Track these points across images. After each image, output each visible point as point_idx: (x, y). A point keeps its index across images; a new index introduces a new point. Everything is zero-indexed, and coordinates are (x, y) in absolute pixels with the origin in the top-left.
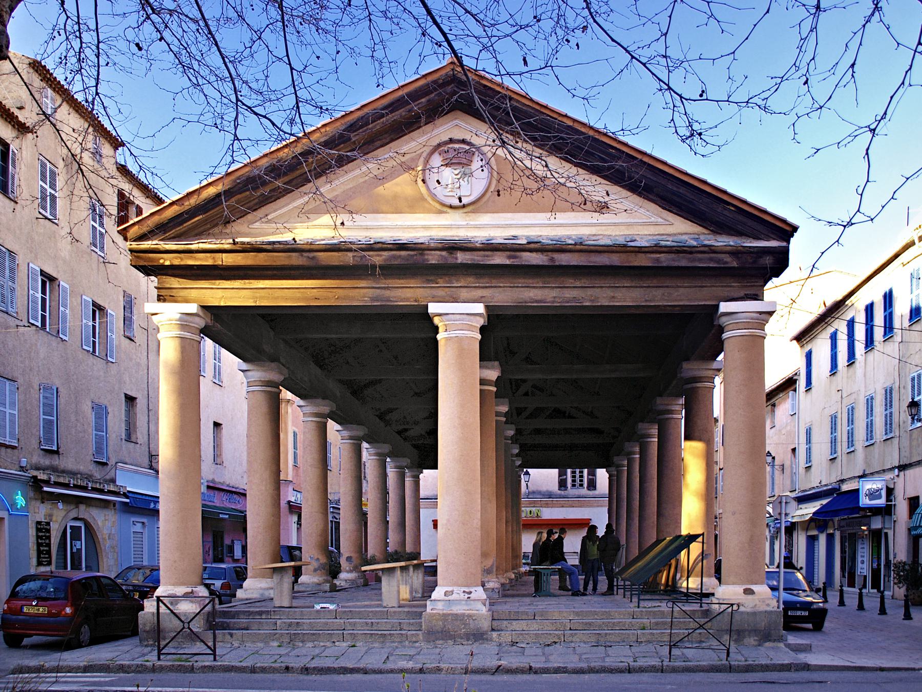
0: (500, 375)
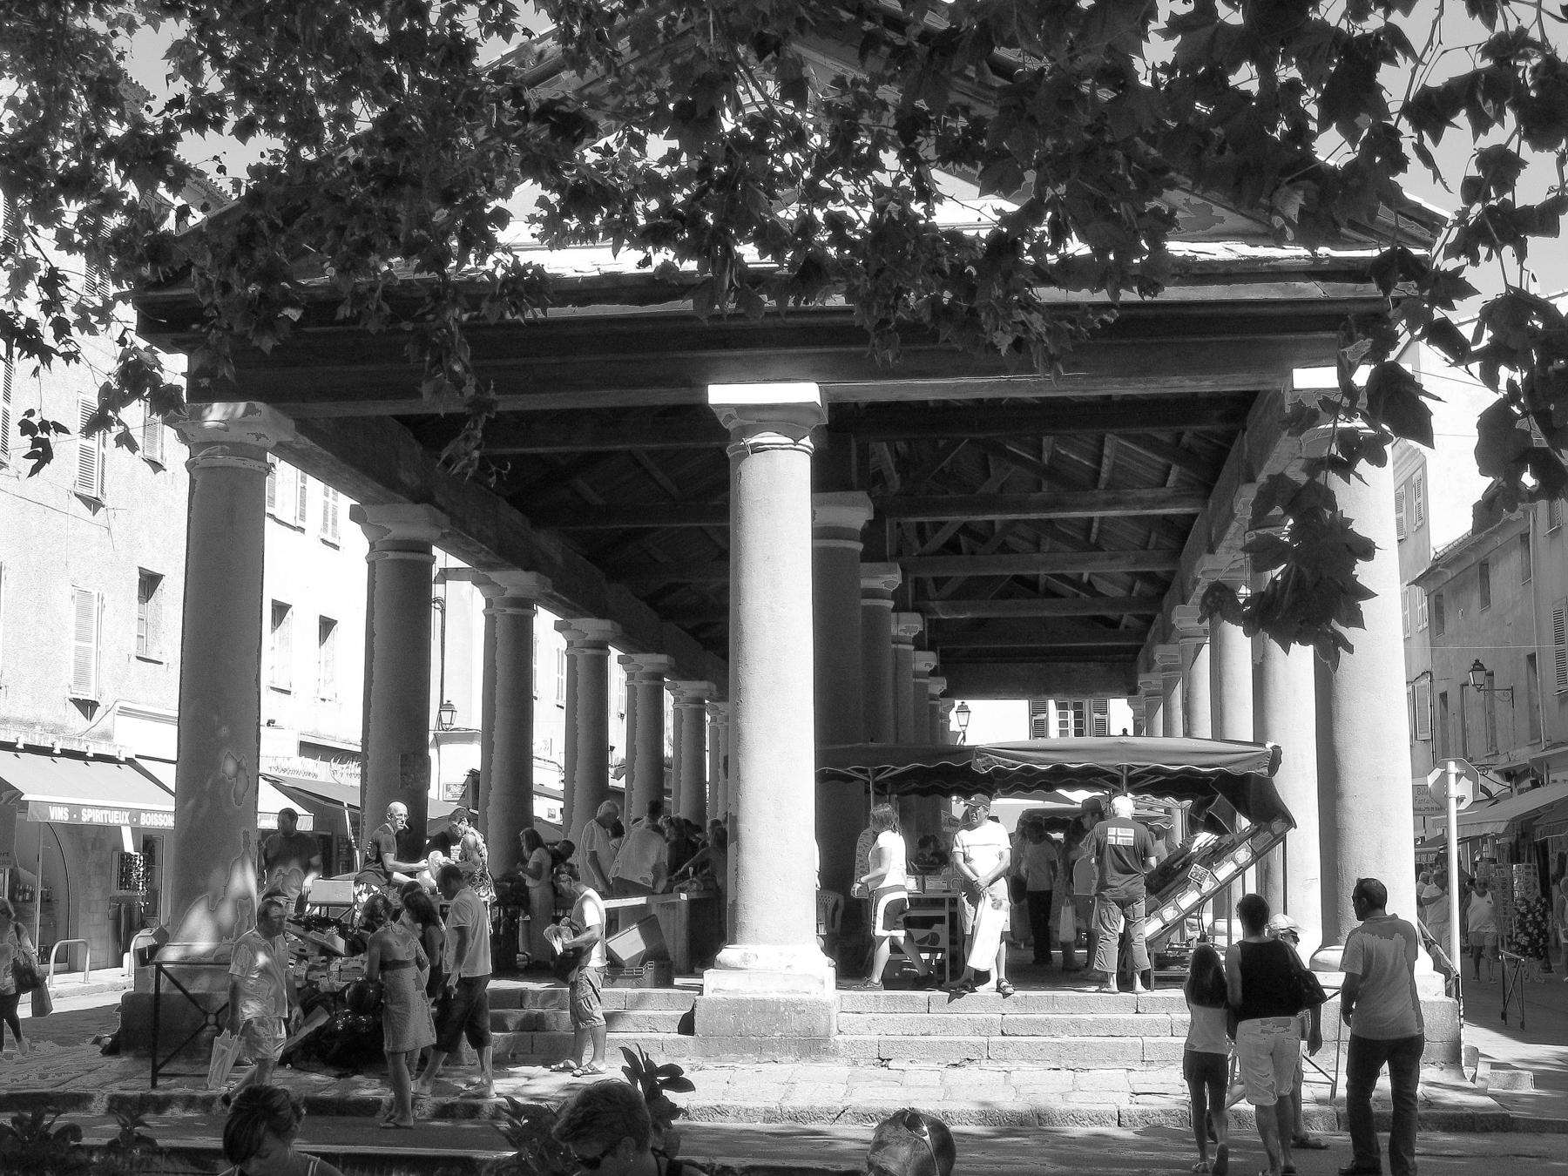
0: (872, 518)
